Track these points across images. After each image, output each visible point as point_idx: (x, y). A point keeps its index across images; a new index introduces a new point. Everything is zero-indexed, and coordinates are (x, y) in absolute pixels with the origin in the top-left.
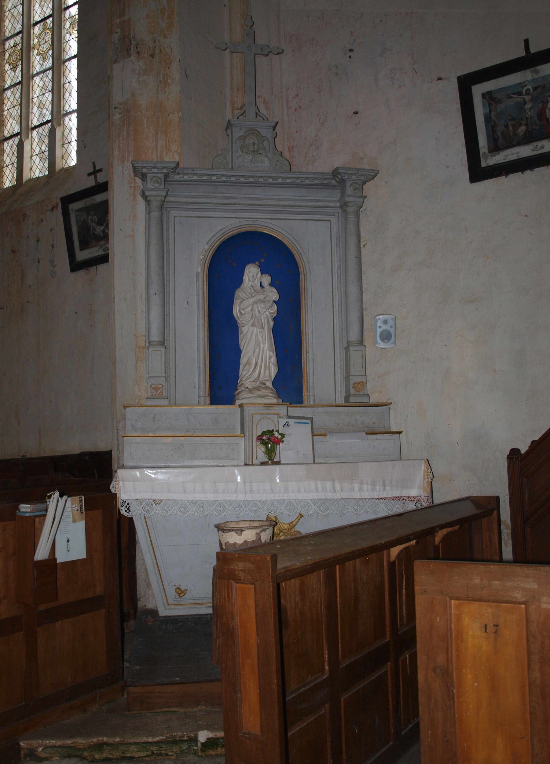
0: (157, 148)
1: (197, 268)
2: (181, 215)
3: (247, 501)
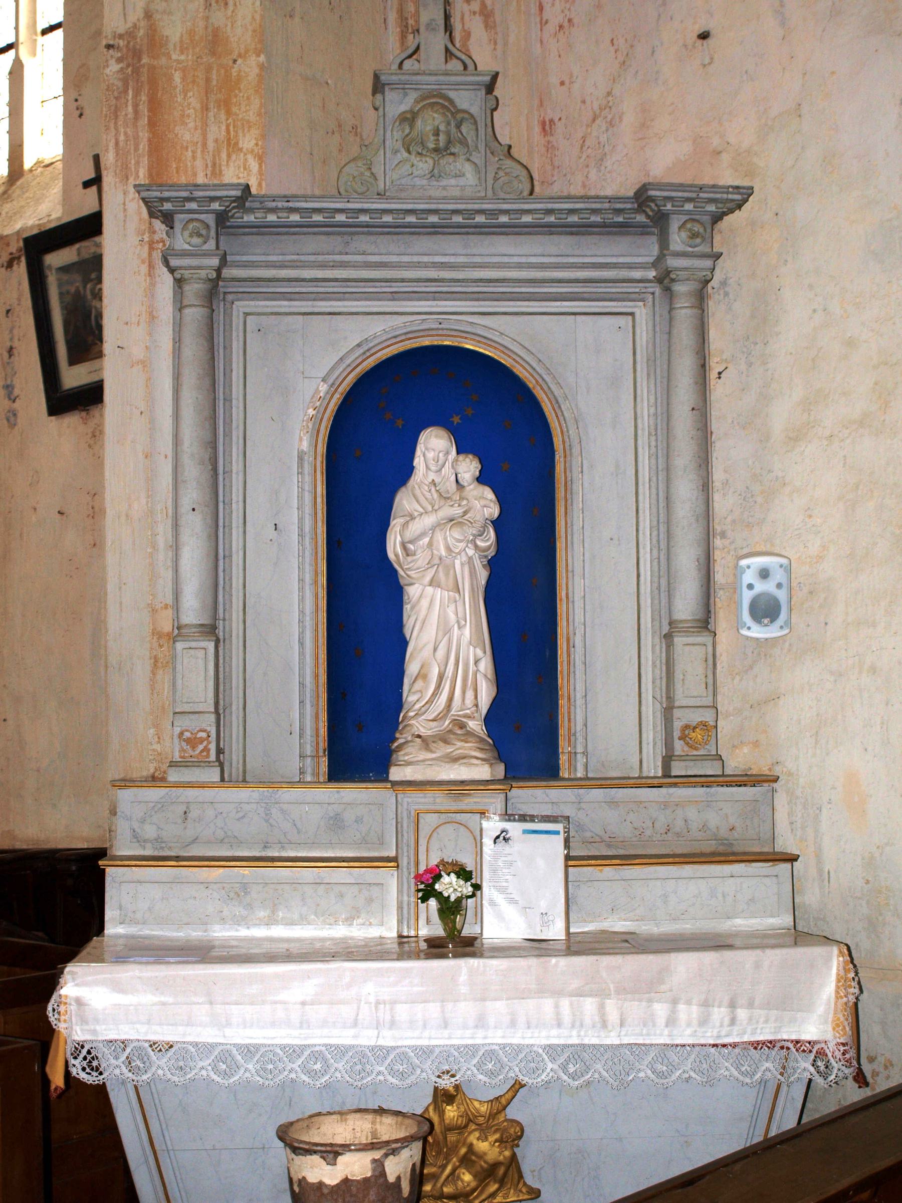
0: (204, 145)
1: (301, 439)
2: (260, 310)
3: (381, 1048)
